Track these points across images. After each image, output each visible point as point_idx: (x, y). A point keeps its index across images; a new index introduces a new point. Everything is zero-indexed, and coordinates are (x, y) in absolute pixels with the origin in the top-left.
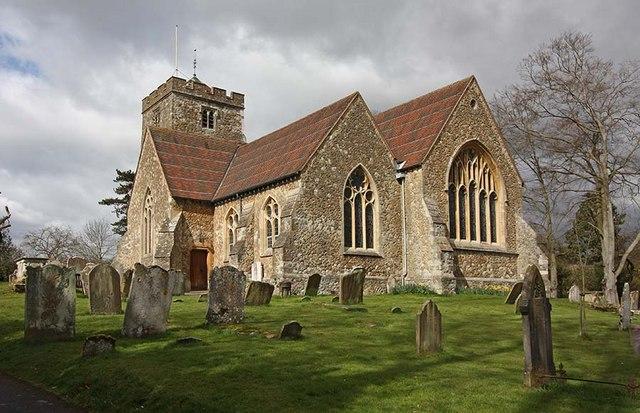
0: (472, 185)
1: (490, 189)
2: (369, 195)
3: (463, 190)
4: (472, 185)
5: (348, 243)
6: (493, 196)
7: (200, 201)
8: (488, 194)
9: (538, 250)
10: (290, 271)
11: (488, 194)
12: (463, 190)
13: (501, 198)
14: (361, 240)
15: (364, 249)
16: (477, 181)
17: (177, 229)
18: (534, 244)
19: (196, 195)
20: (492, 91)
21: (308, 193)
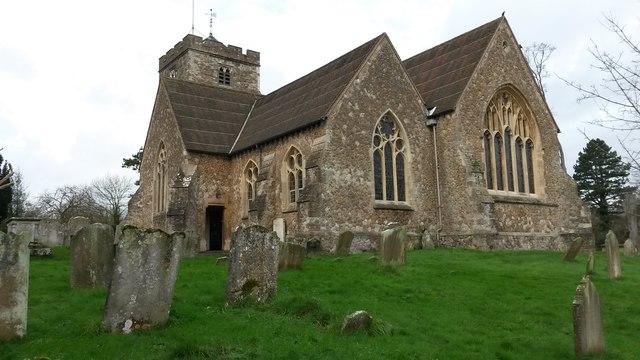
0: (508, 131)
2: (400, 143)
3: (498, 136)
4: (508, 131)
5: (379, 196)
12: (498, 136)
13: (537, 143)
15: (396, 202)
16: (513, 128)
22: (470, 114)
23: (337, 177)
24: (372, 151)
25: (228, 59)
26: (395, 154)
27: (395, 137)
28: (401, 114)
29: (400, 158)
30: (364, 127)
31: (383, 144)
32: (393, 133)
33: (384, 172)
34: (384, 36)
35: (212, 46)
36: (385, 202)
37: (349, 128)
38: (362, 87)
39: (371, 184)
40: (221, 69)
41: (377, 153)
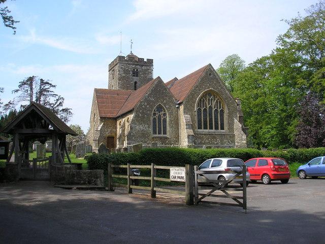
0: (210, 108)
1: (220, 108)
2: (165, 115)
3: (205, 110)
4: (210, 108)
5: (155, 132)
6: (222, 111)
7: (111, 118)
8: (219, 110)
9: (242, 132)
10: (130, 144)
11: (219, 110)
12: (205, 110)
13: (226, 111)
14: (207, 126)
15: (162, 135)
16: (213, 106)
17: (101, 129)
18: (241, 130)
19: (109, 115)
20: (216, 67)
21: (136, 117)
22: (190, 102)
23: (137, 127)
24: (152, 118)
25: (136, 65)
26: (162, 119)
27: (163, 112)
28: (165, 104)
29: (165, 121)
30: (149, 110)
31: (157, 115)
32: (162, 111)
33: (202, 115)
34: (159, 77)
35: (132, 58)
36: (157, 135)
37: (143, 111)
38: (148, 97)
39: (151, 130)
40: (134, 70)
41: (155, 119)
